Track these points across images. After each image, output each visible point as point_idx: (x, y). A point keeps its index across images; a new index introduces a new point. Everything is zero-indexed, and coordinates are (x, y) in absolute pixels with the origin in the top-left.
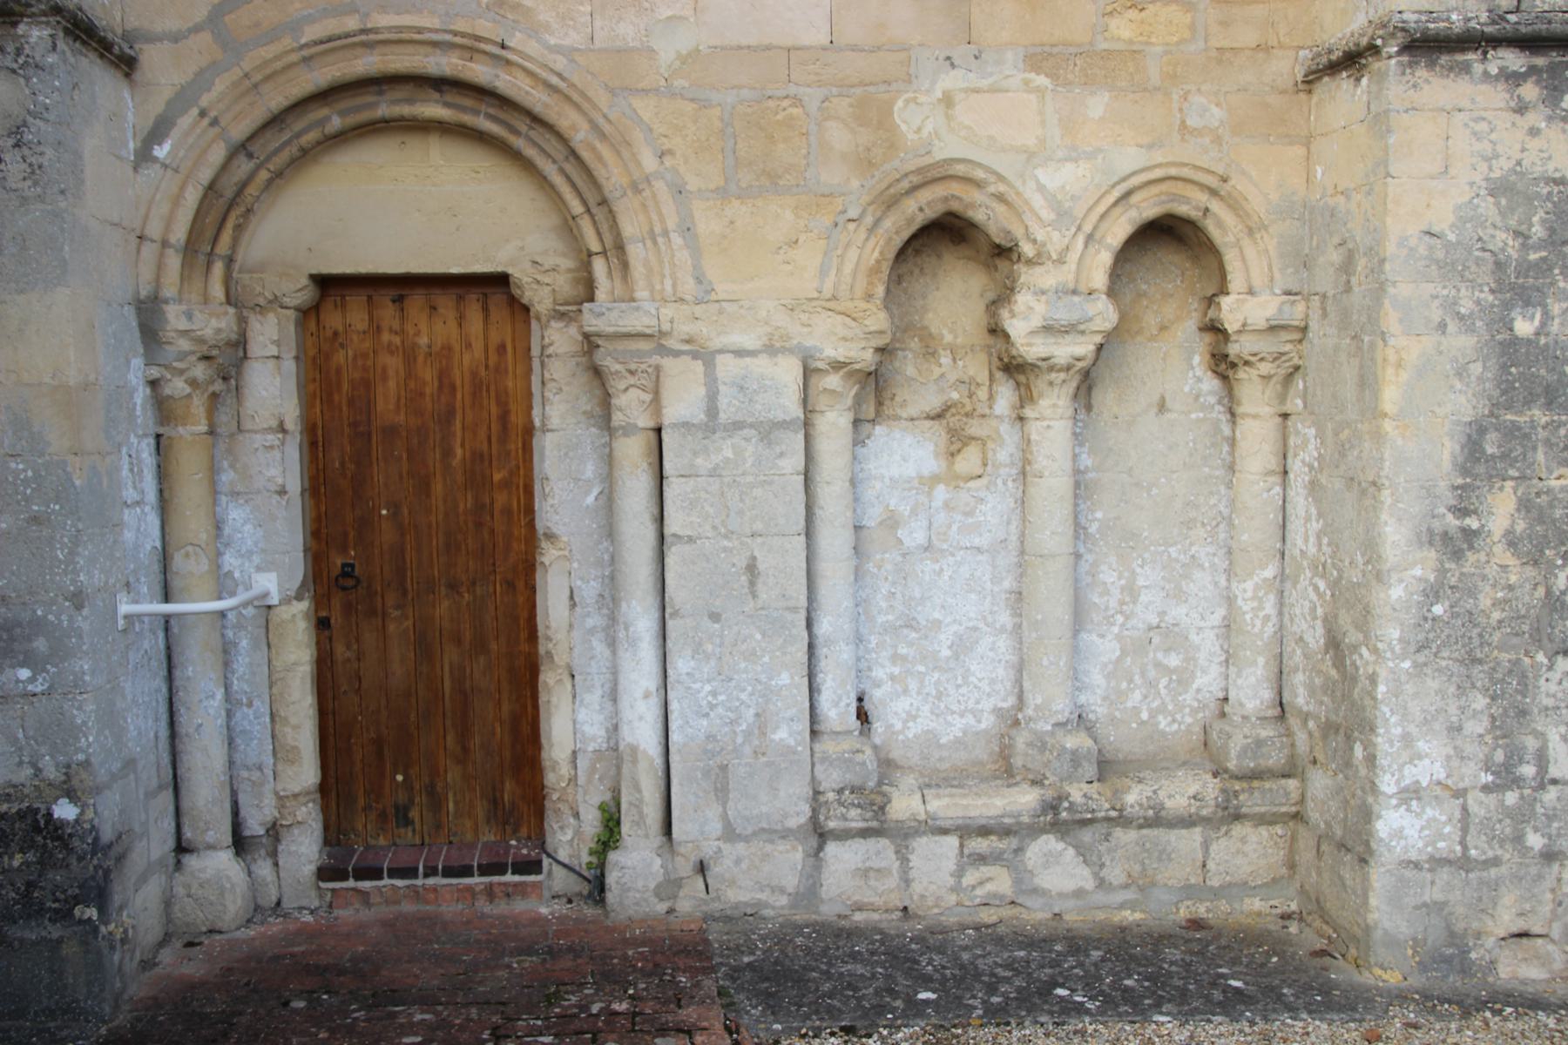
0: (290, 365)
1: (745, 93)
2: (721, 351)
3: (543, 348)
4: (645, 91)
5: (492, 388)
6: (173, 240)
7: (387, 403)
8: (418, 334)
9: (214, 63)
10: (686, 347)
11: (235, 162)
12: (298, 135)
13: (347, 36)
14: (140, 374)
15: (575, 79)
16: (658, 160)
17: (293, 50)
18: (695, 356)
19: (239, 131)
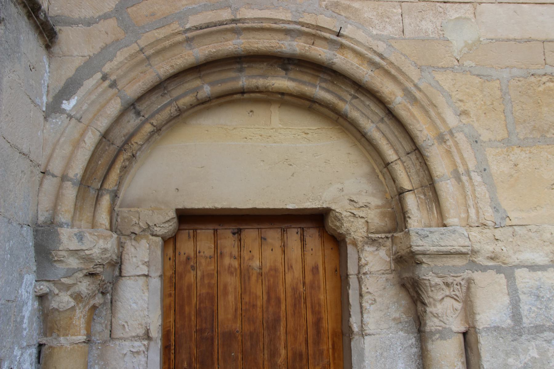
0: (156, 283)
1: (515, 71)
2: (518, 266)
3: (360, 267)
4: (445, 69)
5: (308, 300)
6: (71, 174)
7: (227, 314)
8: (251, 258)
9: (117, 40)
10: (491, 263)
11: (126, 118)
12: (177, 99)
13: (221, 23)
14: (31, 289)
15: (392, 59)
16: (457, 117)
17: (179, 33)
18: (499, 270)
19: (133, 90)
